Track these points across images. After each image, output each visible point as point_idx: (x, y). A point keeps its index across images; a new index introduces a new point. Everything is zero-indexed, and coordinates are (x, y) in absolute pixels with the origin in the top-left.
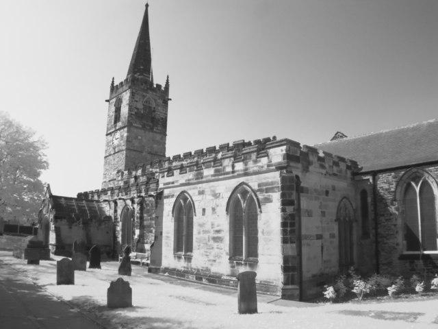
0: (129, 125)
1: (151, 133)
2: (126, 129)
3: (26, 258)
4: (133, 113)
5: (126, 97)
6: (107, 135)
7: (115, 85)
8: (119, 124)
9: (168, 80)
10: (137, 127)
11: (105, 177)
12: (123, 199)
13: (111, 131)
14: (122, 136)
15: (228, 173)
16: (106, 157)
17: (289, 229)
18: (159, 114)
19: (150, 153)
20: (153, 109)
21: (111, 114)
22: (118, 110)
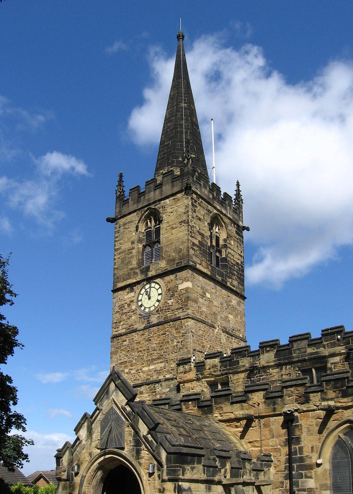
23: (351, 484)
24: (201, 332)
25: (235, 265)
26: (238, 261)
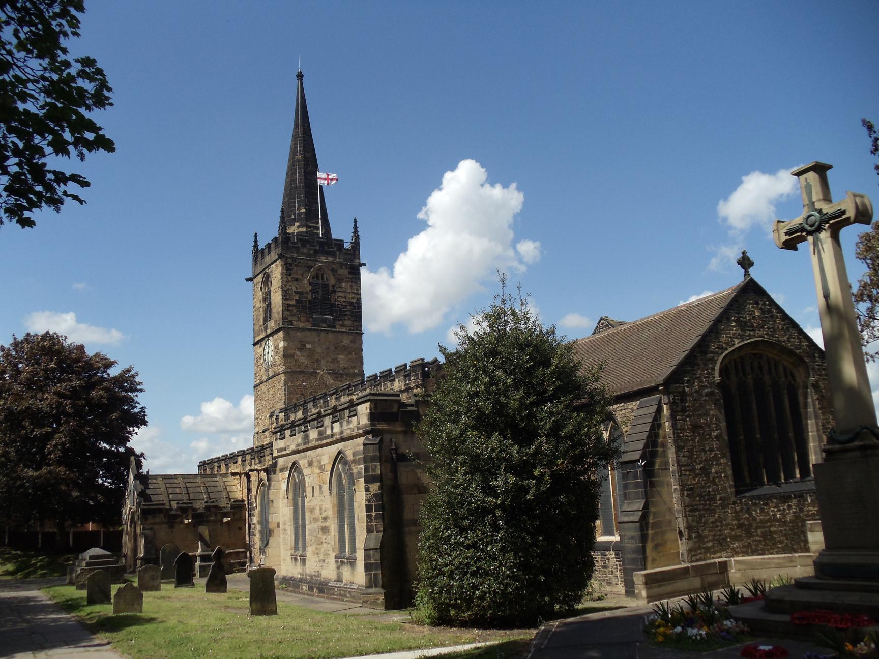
0: (287, 328)
2: (281, 334)
3: (383, 587)
5: (277, 272)
6: (255, 344)
7: (260, 248)
8: (272, 325)
9: (356, 227)
10: (303, 330)
11: (257, 425)
12: (256, 470)
13: (261, 336)
14: (276, 347)
15: (328, 437)
16: (256, 386)
17: (374, 514)
18: (340, 297)
21: (258, 304)
22: (267, 299)
25: (347, 306)
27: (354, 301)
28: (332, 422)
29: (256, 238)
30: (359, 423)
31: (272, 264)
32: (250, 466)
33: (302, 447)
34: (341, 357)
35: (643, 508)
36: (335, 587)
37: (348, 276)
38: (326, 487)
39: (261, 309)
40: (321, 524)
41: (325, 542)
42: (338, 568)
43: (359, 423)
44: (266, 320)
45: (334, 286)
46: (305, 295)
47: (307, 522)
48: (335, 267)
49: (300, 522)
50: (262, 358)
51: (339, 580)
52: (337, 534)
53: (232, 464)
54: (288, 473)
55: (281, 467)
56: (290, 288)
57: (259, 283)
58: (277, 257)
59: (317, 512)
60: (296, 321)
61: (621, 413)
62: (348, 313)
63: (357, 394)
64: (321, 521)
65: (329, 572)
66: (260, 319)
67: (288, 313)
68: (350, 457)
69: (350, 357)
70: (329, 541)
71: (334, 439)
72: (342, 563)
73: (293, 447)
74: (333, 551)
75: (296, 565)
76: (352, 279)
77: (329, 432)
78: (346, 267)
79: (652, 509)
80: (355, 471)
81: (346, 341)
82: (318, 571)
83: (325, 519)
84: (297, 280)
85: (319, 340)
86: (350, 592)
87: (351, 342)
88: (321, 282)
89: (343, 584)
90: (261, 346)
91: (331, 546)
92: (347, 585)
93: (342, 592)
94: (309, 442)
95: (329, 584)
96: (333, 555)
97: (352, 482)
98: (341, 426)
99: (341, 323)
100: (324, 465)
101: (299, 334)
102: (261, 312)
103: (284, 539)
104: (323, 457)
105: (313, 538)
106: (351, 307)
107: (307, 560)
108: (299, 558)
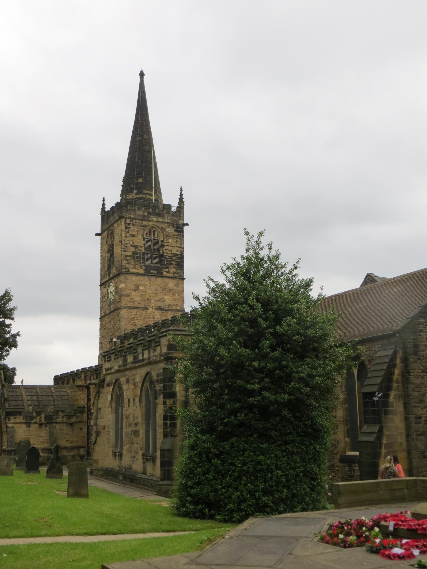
1: (159, 280)
4: (130, 253)
9: (181, 195)
15: (140, 361)
17: (169, 422)
19: (160, 309)
20: (160, 243)
23: (14, 406)
24: (133, 316)
25: (172, 257)
26: (177, 253)
27: (178, 253)
28: (143, 350)
29: (104, 202)
30: (161, 352)
31: (115, 223)
32: (90, 380)
33: (122, 368)
34: (166, 297)
35: (378, 431)
36: (141, 478)
37: (174, 233)
38: (137, 399)
39: (106, 258)
40: (133, 428)
41: (136, 443)
42: (144, 463)
43: (161, 352)
44: (109, 267)
45: (162, 241)
46: (139, 248)
47: (124, 427)
48: (164, 226)
49: (120, 426)
50: (106, 296)
51: (144, 473)
52: (144, 437)
53: (77, 379)
54: (112, 387)
55: (108, 382)
56: (128, 242)
57: (105, 237)
58: (118, 218)
59: (131, 419)
60: (132, 268)
61: (366, 353)
62: (173, 263)
63: (296, 314)
64: (133, 426)
65: (138, 466)
66: (105, 266)
67: (126, 262)
68: (155, 378)
69: (174, 297)
70: (139, 442)
71: (144, 362)
72: (147, 459)
73: (116, 368)
74: (141, 450)
75: (115, 459)
76: (177, 235)
77: (140, 357)
78: (173, 226)
79: (386, 433)
80: (158, 388)
81: (171, 284)
82: (131, 465)
83: (136, 424)
84: (133, 236)
85: (150, 284)
86: (151, 483)
87: (175, 285)
88: (153, 238)
89: (147, 476)
90: (105, 287)
91: (140, 446)
92: (149, 477)
93: (146, 483)
94: (127, 365)
95: (137, 476)
96: (141, 453)
97: (156, 398)
98: (149, 353)
99: (167, 270)
100: (137, 383)
101: (134, 278)
102: (106, 261)
103: (108, 439)
104: (136, 376)
105: (128, 439)
106: (176, 258)
107: (123, 456)
108: (117, 454)
